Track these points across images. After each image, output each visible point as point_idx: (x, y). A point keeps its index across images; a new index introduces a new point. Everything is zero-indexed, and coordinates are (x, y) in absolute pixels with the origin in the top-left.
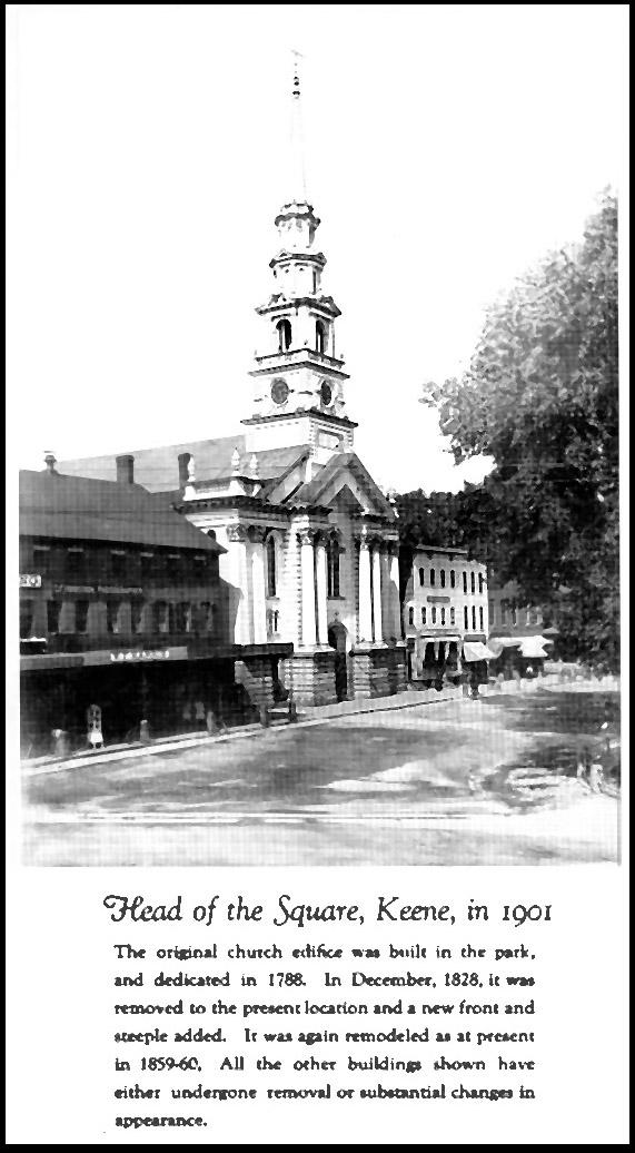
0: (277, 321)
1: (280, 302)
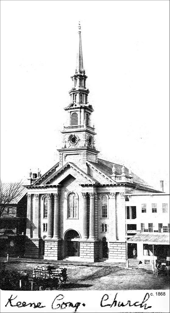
0: (72, 113)
1: (74, 107)
